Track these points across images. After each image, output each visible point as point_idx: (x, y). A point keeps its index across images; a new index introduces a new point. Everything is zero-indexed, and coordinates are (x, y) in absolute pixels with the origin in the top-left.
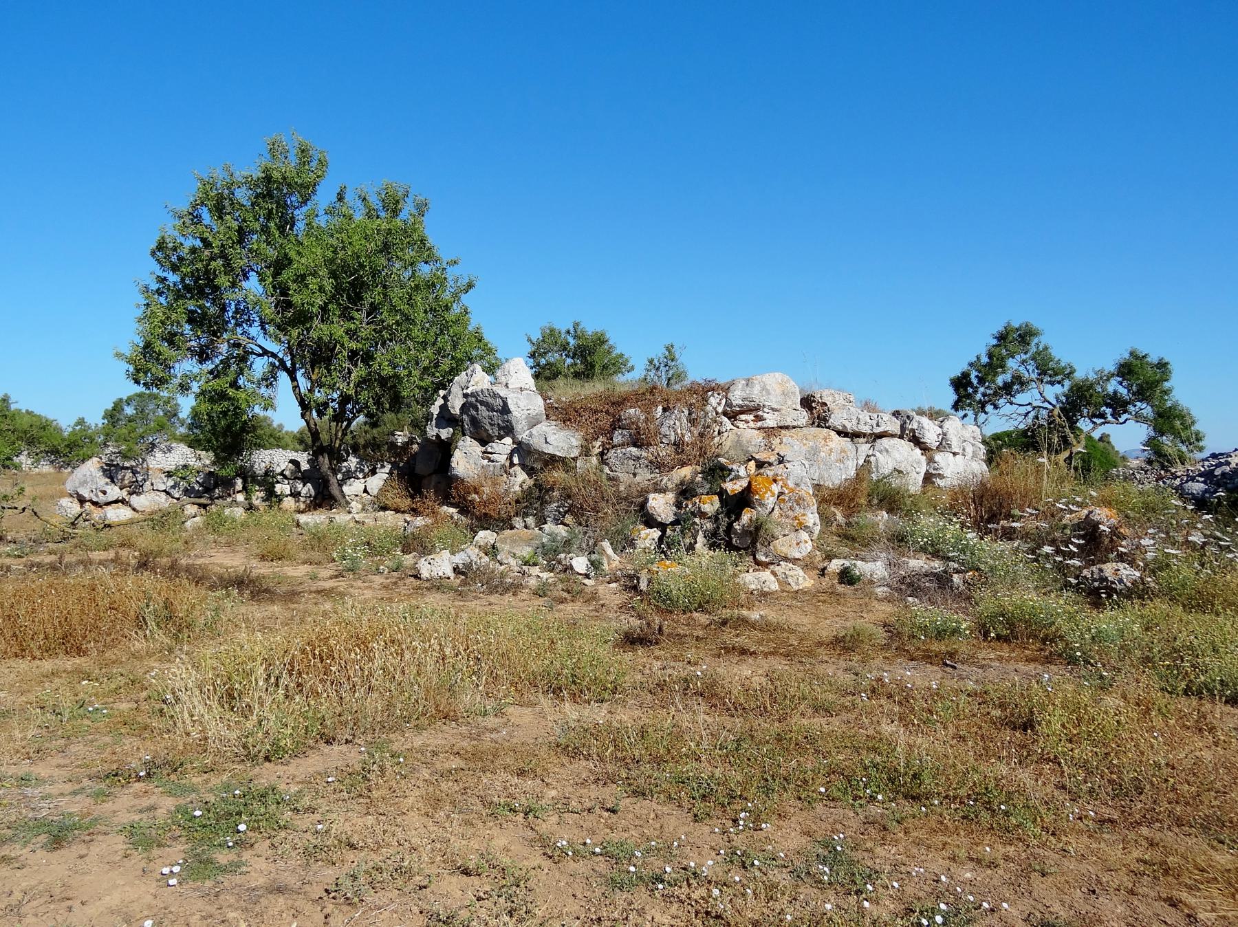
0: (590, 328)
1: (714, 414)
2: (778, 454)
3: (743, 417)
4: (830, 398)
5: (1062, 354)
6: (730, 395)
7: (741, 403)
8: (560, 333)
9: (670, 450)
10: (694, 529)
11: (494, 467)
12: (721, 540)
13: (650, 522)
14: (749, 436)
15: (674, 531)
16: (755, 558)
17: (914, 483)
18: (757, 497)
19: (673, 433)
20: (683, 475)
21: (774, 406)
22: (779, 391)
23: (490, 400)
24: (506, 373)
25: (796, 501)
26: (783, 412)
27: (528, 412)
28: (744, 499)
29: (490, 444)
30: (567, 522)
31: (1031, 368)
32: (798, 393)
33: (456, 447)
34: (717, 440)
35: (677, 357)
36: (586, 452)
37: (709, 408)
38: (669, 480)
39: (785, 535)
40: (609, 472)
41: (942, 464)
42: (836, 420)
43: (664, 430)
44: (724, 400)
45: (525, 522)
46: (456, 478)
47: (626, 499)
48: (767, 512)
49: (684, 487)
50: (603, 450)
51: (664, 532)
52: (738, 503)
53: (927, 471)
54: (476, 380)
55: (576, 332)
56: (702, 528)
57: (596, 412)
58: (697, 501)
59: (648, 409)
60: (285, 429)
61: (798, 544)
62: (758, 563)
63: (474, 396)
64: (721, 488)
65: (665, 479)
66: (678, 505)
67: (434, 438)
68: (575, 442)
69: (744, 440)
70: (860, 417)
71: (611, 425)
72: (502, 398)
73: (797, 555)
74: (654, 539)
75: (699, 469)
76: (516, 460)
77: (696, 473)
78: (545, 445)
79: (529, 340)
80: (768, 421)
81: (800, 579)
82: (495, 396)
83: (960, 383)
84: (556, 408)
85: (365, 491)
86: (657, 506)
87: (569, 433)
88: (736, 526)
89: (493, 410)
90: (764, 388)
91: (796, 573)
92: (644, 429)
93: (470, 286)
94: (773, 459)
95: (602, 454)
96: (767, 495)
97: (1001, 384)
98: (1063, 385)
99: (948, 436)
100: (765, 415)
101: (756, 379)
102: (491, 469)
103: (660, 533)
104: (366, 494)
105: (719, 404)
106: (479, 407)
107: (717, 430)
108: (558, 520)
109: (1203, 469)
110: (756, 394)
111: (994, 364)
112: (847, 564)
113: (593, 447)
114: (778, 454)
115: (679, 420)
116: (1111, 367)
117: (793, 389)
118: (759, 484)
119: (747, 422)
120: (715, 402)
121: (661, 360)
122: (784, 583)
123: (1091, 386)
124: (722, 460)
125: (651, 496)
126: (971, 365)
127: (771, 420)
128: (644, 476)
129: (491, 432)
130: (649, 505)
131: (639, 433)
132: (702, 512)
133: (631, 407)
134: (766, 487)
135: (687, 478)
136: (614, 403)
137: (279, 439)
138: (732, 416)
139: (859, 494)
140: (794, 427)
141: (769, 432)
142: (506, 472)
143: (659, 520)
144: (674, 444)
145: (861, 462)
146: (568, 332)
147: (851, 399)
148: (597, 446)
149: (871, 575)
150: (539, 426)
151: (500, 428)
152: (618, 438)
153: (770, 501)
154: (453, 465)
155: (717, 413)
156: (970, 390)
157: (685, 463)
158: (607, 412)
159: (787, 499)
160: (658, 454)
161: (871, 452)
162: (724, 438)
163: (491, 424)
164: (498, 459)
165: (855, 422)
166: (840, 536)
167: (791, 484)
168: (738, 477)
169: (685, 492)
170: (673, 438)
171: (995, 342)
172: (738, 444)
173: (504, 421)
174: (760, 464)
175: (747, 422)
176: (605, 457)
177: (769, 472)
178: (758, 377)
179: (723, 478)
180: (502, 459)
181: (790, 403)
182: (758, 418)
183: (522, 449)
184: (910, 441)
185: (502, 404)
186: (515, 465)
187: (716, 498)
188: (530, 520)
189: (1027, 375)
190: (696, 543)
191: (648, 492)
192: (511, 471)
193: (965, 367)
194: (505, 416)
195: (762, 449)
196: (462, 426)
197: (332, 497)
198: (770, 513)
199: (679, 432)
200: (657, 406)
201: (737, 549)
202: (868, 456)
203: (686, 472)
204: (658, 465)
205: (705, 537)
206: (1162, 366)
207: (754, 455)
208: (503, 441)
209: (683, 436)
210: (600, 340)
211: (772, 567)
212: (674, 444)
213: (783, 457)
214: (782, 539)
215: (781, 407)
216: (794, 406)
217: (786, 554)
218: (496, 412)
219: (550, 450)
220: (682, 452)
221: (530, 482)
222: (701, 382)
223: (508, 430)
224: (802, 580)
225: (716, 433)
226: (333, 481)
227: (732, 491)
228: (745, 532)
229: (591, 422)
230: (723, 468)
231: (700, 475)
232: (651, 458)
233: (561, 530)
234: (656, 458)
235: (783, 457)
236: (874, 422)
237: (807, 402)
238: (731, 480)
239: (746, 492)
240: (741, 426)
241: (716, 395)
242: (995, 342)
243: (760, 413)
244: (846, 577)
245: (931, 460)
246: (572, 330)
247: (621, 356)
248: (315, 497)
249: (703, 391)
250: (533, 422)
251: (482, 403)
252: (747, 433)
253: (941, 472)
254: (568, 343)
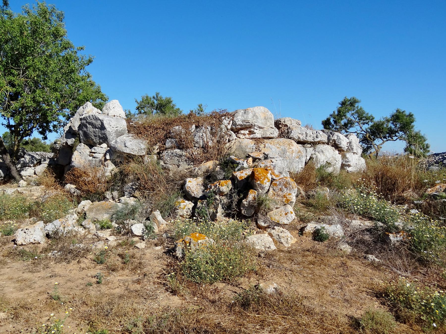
0: (164, 96)
1: (226, 129)
2: (264, 153)
3: (242, 132)
4: (289, 122)
5: (368, 110)
6: (235, 119)
7: (241, 123)
8: (150, 98)
9: (200, 151)
10: (216, 203)
11: (95, 161)
12: (234, 211)
13: (187, 196)
14: (246, 143)
15: (202, 204)
16: (257, 223)
18: (259, 182)
19: (201, 141)
20: (208, 166)
21: (260, 125)
22: (262, 117)
23: (94, 121)
24: (108, 108)
25: (284, 185)
26: (265, 129)
27: (117, 129)
29: (94, 148)
30: (136, 196)
31: (355, 116)
32: (273, 118)
33: (76, 150)
34: (228, 145)
35: (204, 110)
36: (149, 153)
37: (223, 126)
38: (199, 169)
39: (277, 208)
40: (163, 164)
41: (350, 159)
42: (295, 134)
43: (196, 139)
44: (232, 121)
45: (112, 194)
46: (74, 166)
47: (173, 180)
48: (265, 192)
49: (209, 174)
50: (160, 151)
51: (196, 204)
53: (342, 163)
54: (88, 110)
55: (157, 97)
56: (221, 202)
57: (157, 129)
58: (218, 184)
60: (47, 144)
61: (286, 214)
62: (259, 227)
63: (85, 120)
64: (233, 175)
65: (197, 169)
66: (205, 186)
67: (65, 144)
68: (143, 146)
69: (243, 145)
70: (307, 132)
71: (165, 136)
72: (100, 120)
73: (286, 222)
74: (189, 209)
75: (217, 162)
76: (108, 157)
77: (216, 165)
78: (124, 148)
79: (136, 101)
80: (256, 134)
81: (289, 239)
82: (97, 119)
83: (326, 124)
84: (135, 127)
85: (35, 173)
86: (192, 186)
87: (140, 141)
88: (244, 202)
89: (96, 128)
90: (255, 115)
91: (286, 234)
92: (184, 138)
93: (90, 61)
94: (261, 156)
95: (159, 153)
96: (265, 181)
97: (343, 124)
98: (368, 124)
99: (352, 144)
100: (255, 131)
101: (250, 110)
102: (94, 162)
103: (193, 205)
104: (35, 175)
105: (229, 124)
106: (88, 126)
107: (227, 139)
108: (131, 194)
109: (435, 160)
110: (250, 118)
111: (340, 114)
112: (319, 226)
113: (154, 149)
114: (264, 153)
115: (205, 133)
116: (389, 117)
117: (271, 116)
118: (260, 174)
119: (244, 135)
120: (226, 123)
121: (196, 111)
122: (277, 242)
123: (383, 124)
124: (233, 157)
125: (188, 180)
126: (331, 115)
127: (258, 134)
128: (184, 167)
129: (95, 140)
130: (186, 185)
131: (181, 141)
132: (221, 192)
133: (177, 125)
134: (264, 176)
135: (210, 168)
136: (167, 124)
137: (44, 148)
138: (236, 132)
139: (312, 177)
140: (272, 138)
141: (258, 141)
142: (102, 164)
143: (193, 195)
144: (202, 147)
145: (308, 158)
146: (154, 98)
147: (300, 123)
148: (156, 148)
149: (334, 234)
150: (122, 136)
151: (100, 138)
152: (168, 144)
153: (267, 185)
154: (73, 160)
155: (227, 129)
156: (330, 126)
157: (209, 159)
158: (163, 129)
159: (278, 183)
160: (193, 153)
161: (313, 152)
162: (232, 144)
163: (95, 136)
164: (98, 157)
165: (304, 136)
166: (304, 204)
167: (276, 172)
168: (243, 168)
170: (201, 144)
171: (340, 106)
172: (240, 147)
173: (102, 134)
174: (254, 160)
175: (244, 135)
176: (161, 155)
177: (262, 165)
178: (251, 108)
179: (233, 168)
180: (100, 156)
181: (269, 124)
182: (251, 133)
183: (112, 151)
184: (332, 146)
185: (100, 124)
186: (108, 160)
187: (230, 182)
188: (115, 193)
189: (354, 119)
190: (217, 212)
191: (186, 177)
192: (105, 163)
193: (328, 116)
194: (103, 131)
195: (254, 150)
196: (79, 137)
197: (14, 178)
198: (267, 193)
199: (205, 140)
200: (192, 125)
201: (245, 217)
202: (312, 154)
203: (210, 164)
204: (192, 160)
205: (223, 208)
206: (411, 116)
207: (250, 154)
208: (101, 146)
209: (208, 142)
210: (169, 102)
211: (269, 230)
212: (202, 147)
213: (267, 155)
214: (275, 210)
215: (264, 126)
216: (271, 126)
217: (278, 221)
218: (98, 128)
219: (127, 151)
220: (207, 152)
221: (116, 170)
222: (218, 111)
223: (104, 139)
225: (227, 141)
226: (13, 168)
227: (240, 177)
228: (251, 206)
229: (153, 135)
230: (233, 162)
231: (219, 167)
232: (188, 155)
233: (131, 201)
234: (191, 156)
235: (267, 155)
236: (315, 135)
237: (277, 124)
238: (239, 170)
239: (250, 179)
240: (241, 137)
241: (227, 119)
242: (340, 106)
243: (252, 130)
245: (344, 157)
246: (155, 97)
247: (179, 109)
248: (4, 177)
250: (119, 134)
251: (90, 123)
253: (349, 164)
254: (154, 103)
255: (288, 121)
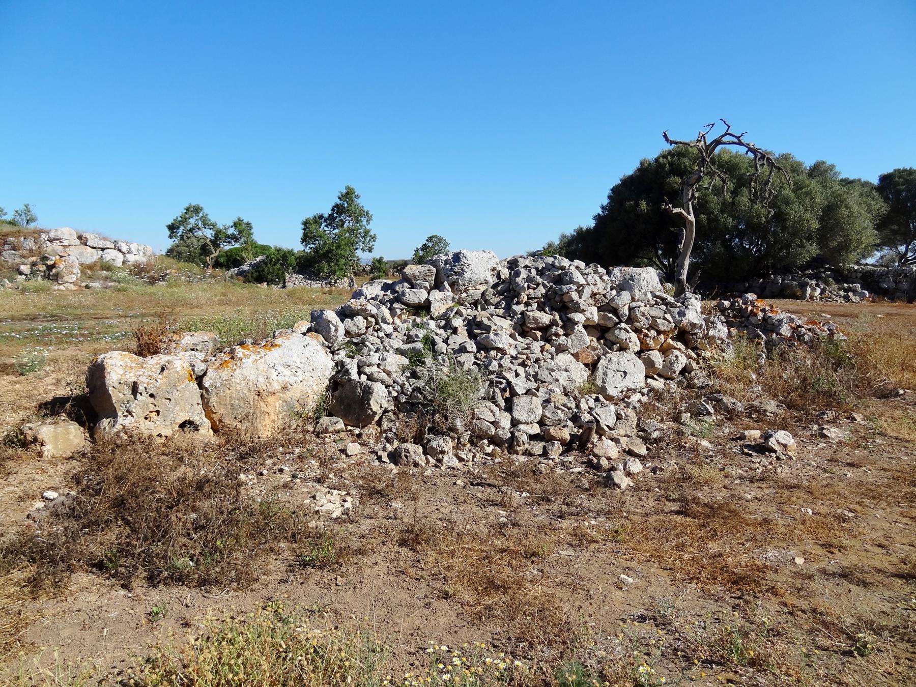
5: (212, 218)
13: (21, 273)
17: (119, 263)
28: (53, 266)
43: (25, 245)
52: (50, 268)
59: (18, 237)
66: (31, 268)
110: (59, 234)
120: (44, 237)
141: (65, 246)
153: (62, 267)
169: (34, 264)
172: (53, 250)
174: (61, 257)
177: (63, 259)
182: (61, 242)
203: (34, 259)
224: (72, 287)
228: (54, 275)
230: (47, 257)
237: (80, 238)
244: (87, 287)
245: (125, 257)
249: (39, 232)
252: (56, 246)
255: (87, 235)
